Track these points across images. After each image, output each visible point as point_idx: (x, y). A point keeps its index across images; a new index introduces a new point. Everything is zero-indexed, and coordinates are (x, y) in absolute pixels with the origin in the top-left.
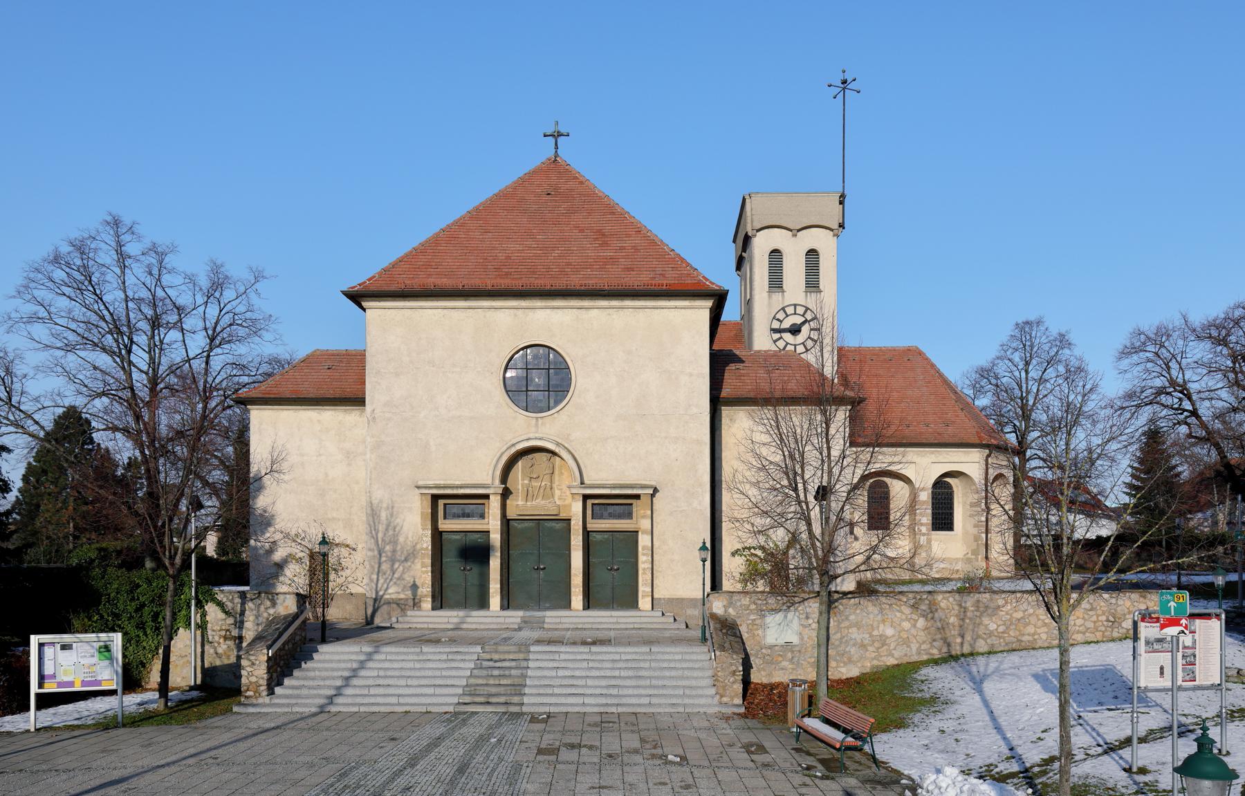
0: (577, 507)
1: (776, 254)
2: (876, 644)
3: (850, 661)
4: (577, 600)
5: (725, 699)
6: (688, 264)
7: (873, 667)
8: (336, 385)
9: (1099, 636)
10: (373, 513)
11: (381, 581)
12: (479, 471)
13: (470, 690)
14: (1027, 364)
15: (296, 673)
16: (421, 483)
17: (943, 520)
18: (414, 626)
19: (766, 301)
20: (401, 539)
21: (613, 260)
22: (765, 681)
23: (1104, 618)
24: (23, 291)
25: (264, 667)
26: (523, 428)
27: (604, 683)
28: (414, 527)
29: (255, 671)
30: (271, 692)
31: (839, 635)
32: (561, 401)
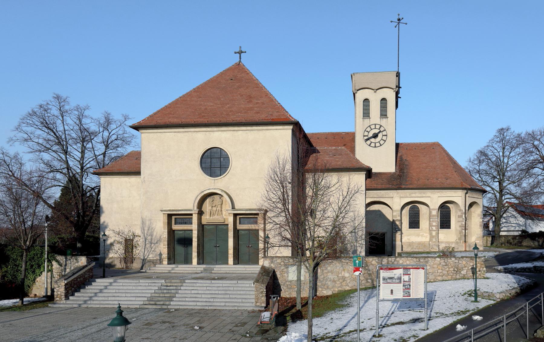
0: (231, 220)
1: (366, 101)
2: (341, 281)
3: (328, 287)
4: (231, 260)
5: (258, 304)
6: (284, 109)
7: (338, 291)
8: (130, 167)
9: (450, 277)
10: (143, 223)
11: (146, 252)
12: (187, 203)
13: (151, 299)
14: (504, 148)
15: (82, 290)
16: (164, 209)
17: (445, 223)
18: (156, 271)
19: (362, 123)
20: (155, 234)
21: (252, 108)
22: (288, 296)
23: (452, 269)
24: (18, 128)
25: (63, 287)
26: (209, 184)
27: (209, 296)
28: (160, 229)
29: (60, 290)
30: (67, 297)
31: (323, 276)
32: (224, 173)
